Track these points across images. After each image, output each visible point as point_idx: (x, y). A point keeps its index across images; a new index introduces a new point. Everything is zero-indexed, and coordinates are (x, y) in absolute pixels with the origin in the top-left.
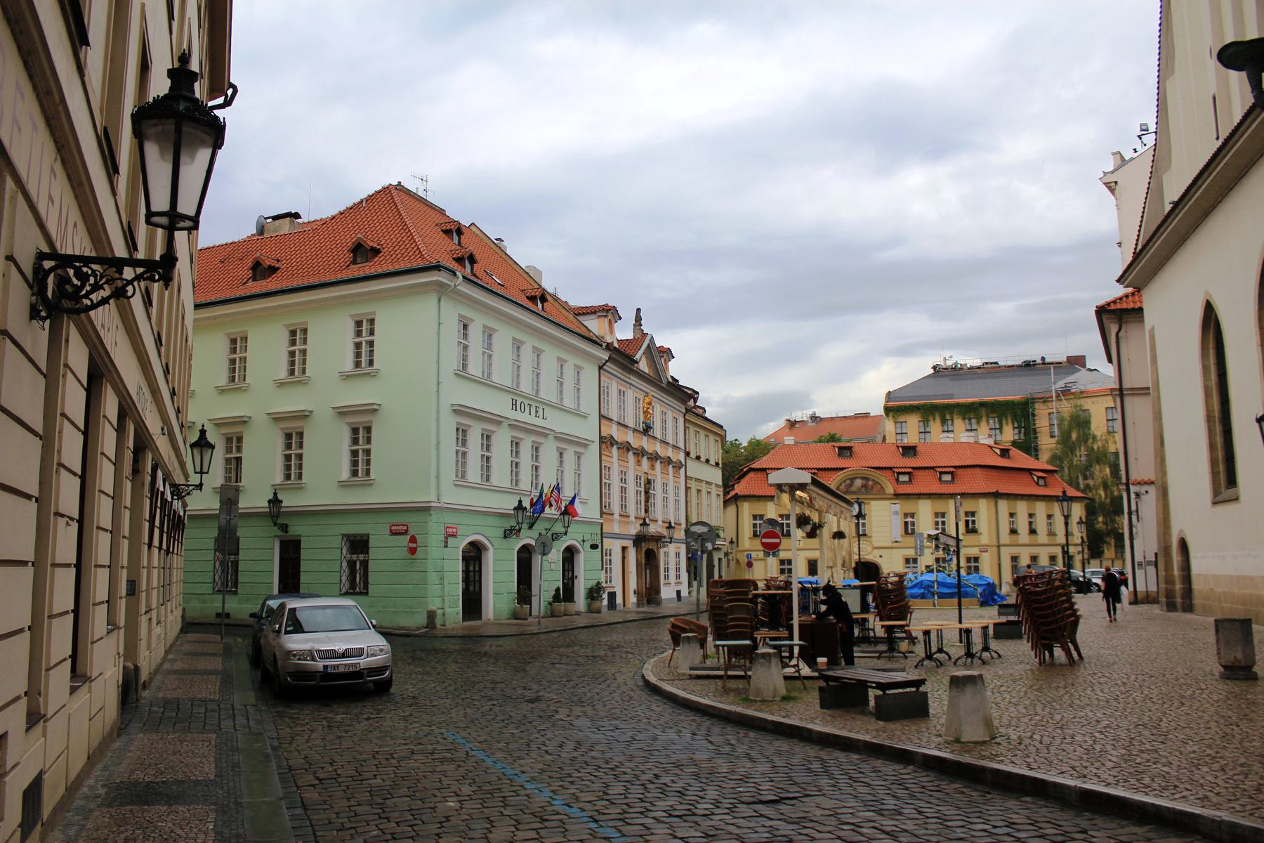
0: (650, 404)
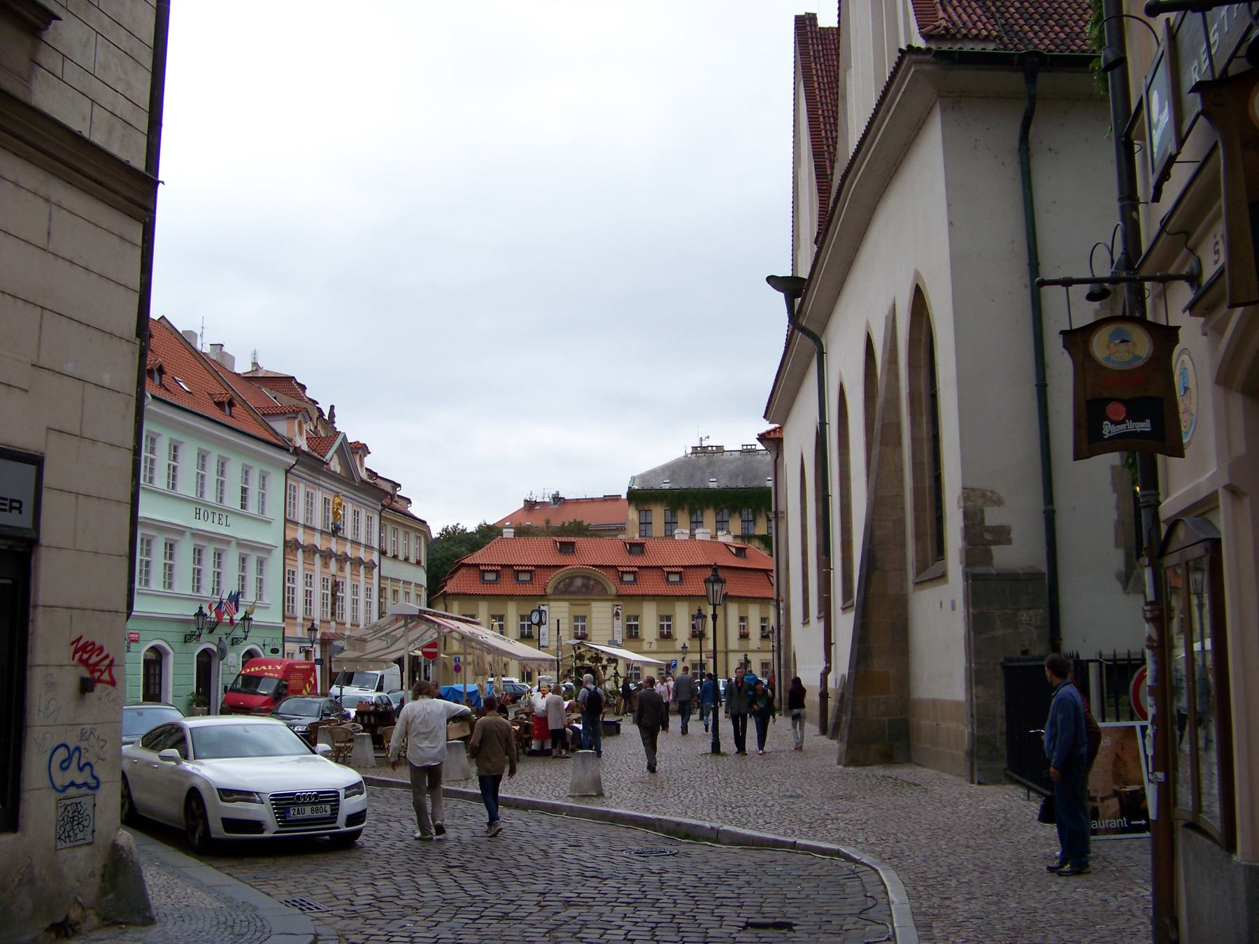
0: (340, 504)
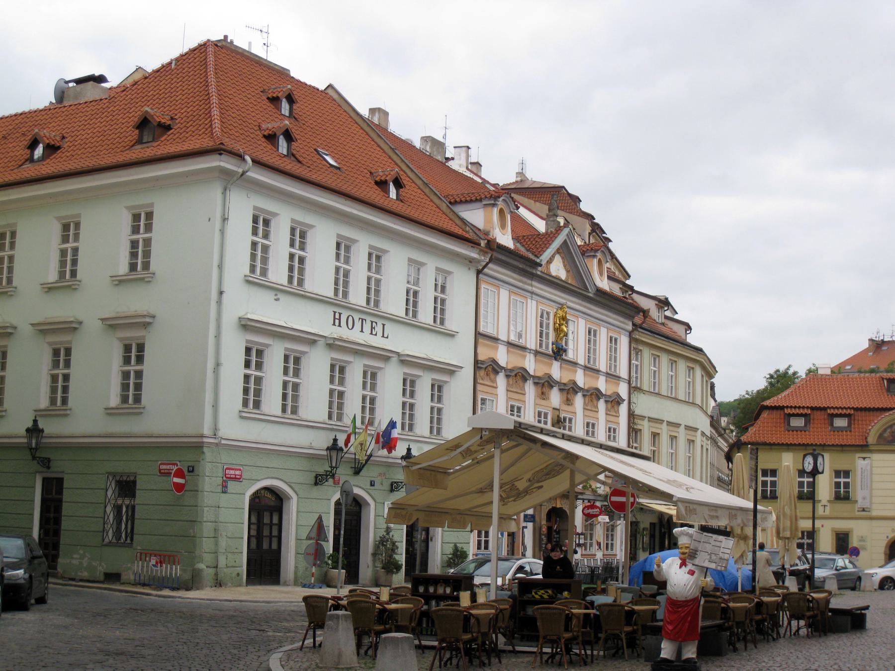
0: (564, 318)
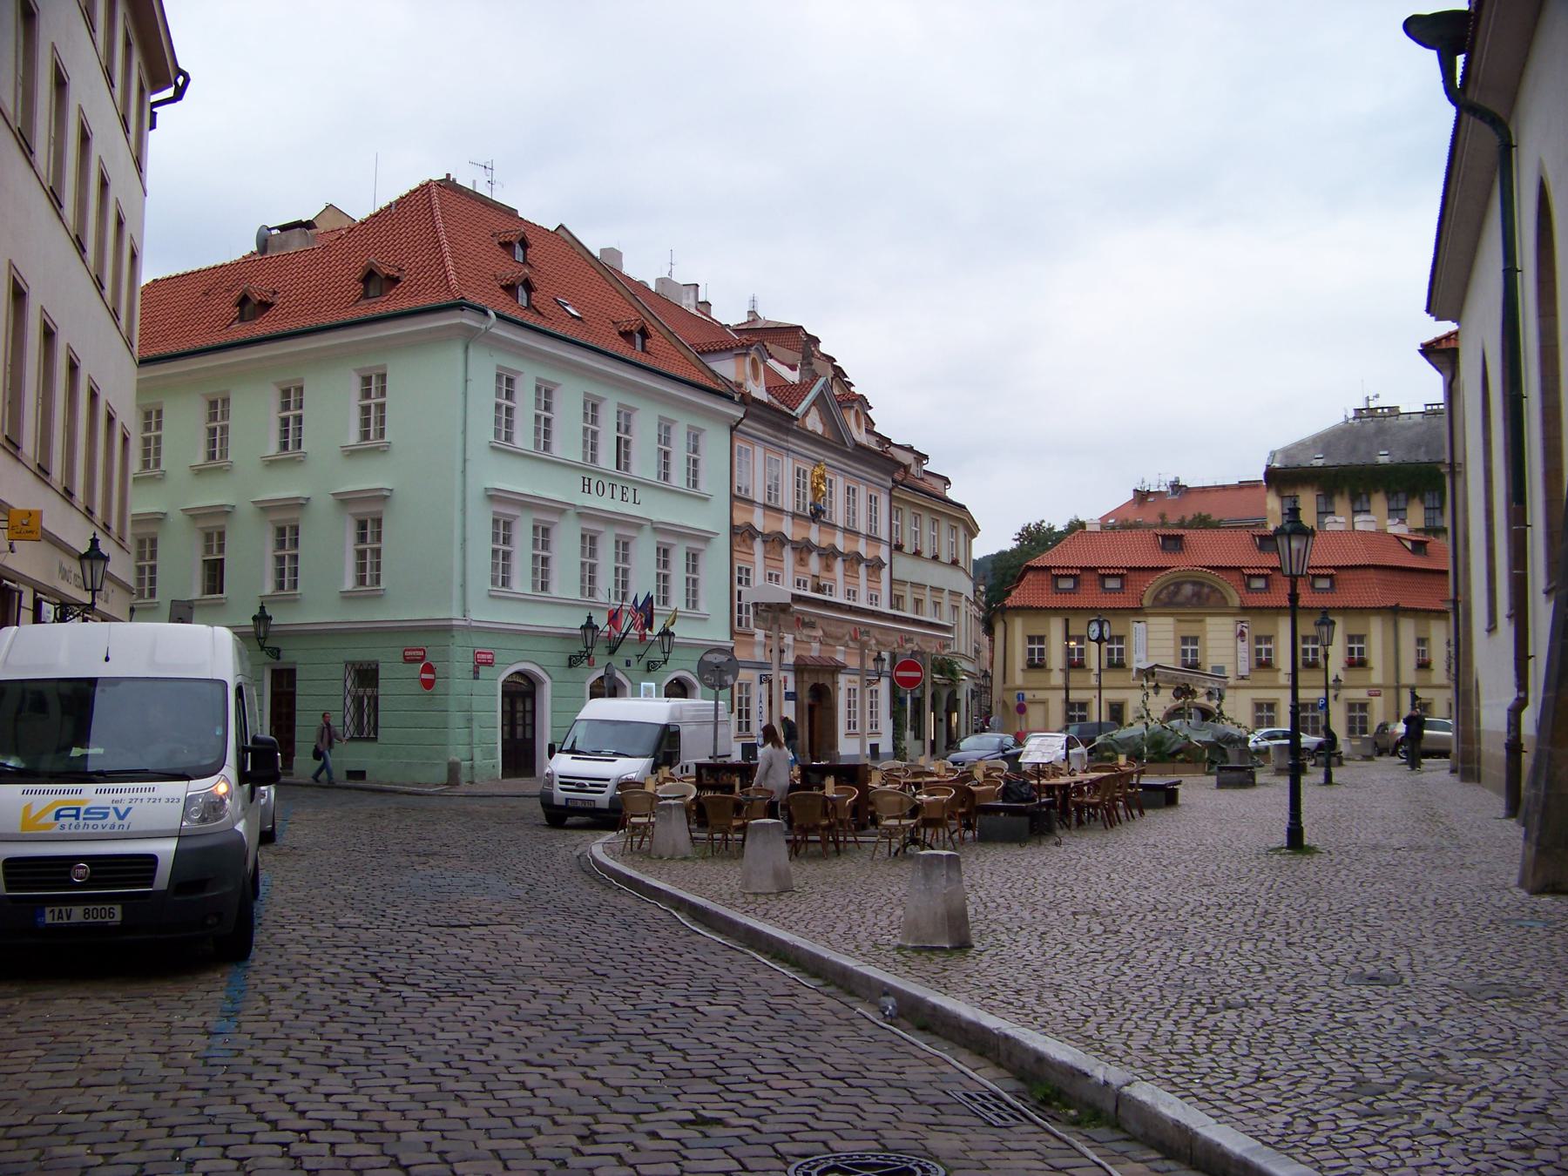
0: (822, 477)
